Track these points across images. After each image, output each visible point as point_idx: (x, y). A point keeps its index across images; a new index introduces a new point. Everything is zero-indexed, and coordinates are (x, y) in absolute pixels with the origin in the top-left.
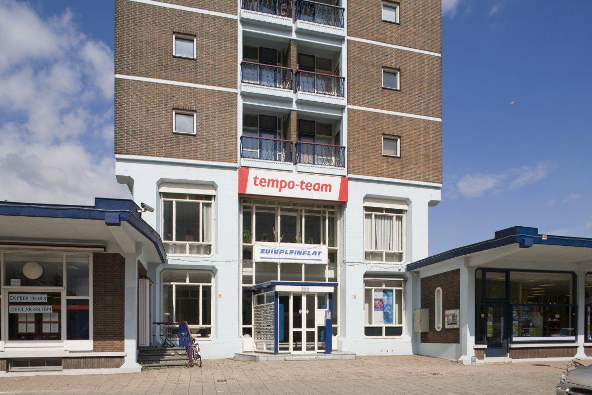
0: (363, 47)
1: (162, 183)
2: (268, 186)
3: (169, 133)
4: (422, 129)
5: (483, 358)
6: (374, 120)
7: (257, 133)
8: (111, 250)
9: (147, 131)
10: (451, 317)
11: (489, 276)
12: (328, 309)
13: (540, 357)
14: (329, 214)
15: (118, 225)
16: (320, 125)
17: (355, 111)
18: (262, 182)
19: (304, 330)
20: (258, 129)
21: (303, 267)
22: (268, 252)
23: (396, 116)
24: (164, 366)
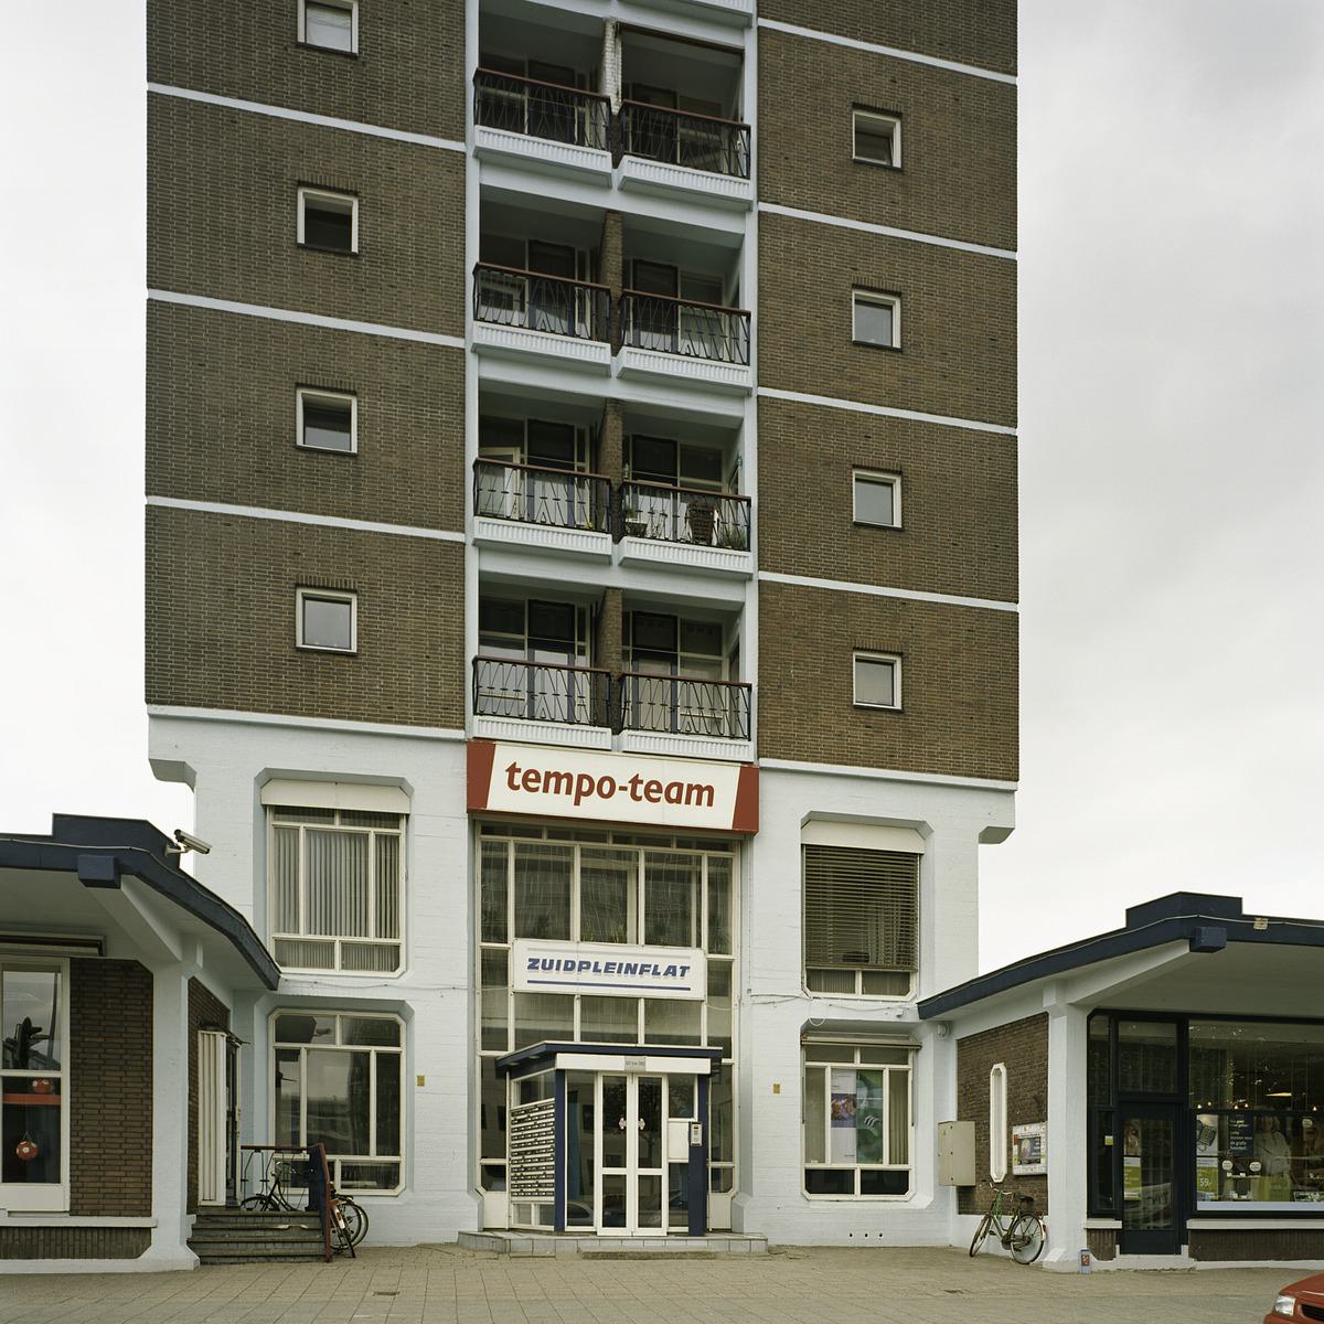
0: (800, 415)
1: (269, 777)
2: (546, 790)
3: (287, 651)
4: (964, 634)
5: (1111, 1256)
6: (830, 612)
7: (523, 649)
8: (116, 953)
9: (228, 644)
10: (1026, 1145)
11: (1130, 1031)
12: (695, 1119)
13: (1278, 1258)
14: (582, 855)
15: (115, 885)
16: (689, 626)
18: (531, 780)
20: (525, 637)
21: (642, 1004)
22: (548, 966)
24: (257, 1256)
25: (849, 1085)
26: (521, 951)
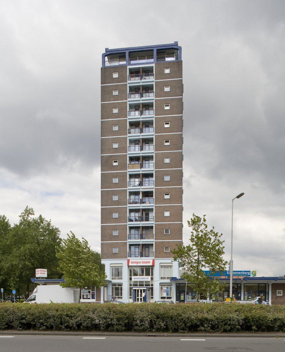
18: (133, 263)
19: (139, 298)
23: (168, 241)
25: (165, 288)
26: (133, 277)
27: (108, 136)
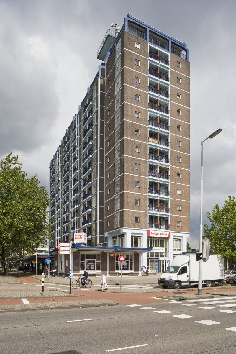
17: (171, 216)
18: (153, 233)
27: (130, 103)
